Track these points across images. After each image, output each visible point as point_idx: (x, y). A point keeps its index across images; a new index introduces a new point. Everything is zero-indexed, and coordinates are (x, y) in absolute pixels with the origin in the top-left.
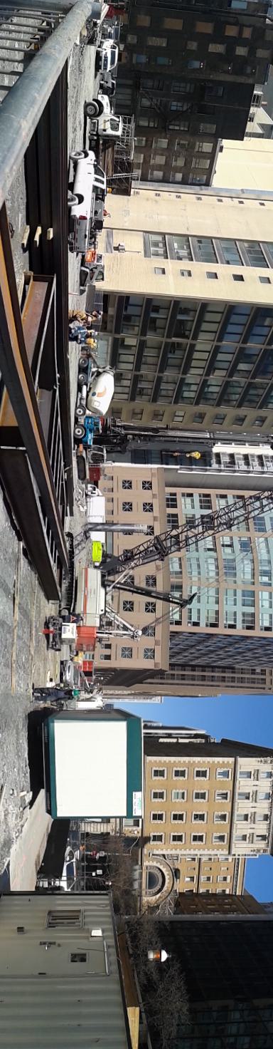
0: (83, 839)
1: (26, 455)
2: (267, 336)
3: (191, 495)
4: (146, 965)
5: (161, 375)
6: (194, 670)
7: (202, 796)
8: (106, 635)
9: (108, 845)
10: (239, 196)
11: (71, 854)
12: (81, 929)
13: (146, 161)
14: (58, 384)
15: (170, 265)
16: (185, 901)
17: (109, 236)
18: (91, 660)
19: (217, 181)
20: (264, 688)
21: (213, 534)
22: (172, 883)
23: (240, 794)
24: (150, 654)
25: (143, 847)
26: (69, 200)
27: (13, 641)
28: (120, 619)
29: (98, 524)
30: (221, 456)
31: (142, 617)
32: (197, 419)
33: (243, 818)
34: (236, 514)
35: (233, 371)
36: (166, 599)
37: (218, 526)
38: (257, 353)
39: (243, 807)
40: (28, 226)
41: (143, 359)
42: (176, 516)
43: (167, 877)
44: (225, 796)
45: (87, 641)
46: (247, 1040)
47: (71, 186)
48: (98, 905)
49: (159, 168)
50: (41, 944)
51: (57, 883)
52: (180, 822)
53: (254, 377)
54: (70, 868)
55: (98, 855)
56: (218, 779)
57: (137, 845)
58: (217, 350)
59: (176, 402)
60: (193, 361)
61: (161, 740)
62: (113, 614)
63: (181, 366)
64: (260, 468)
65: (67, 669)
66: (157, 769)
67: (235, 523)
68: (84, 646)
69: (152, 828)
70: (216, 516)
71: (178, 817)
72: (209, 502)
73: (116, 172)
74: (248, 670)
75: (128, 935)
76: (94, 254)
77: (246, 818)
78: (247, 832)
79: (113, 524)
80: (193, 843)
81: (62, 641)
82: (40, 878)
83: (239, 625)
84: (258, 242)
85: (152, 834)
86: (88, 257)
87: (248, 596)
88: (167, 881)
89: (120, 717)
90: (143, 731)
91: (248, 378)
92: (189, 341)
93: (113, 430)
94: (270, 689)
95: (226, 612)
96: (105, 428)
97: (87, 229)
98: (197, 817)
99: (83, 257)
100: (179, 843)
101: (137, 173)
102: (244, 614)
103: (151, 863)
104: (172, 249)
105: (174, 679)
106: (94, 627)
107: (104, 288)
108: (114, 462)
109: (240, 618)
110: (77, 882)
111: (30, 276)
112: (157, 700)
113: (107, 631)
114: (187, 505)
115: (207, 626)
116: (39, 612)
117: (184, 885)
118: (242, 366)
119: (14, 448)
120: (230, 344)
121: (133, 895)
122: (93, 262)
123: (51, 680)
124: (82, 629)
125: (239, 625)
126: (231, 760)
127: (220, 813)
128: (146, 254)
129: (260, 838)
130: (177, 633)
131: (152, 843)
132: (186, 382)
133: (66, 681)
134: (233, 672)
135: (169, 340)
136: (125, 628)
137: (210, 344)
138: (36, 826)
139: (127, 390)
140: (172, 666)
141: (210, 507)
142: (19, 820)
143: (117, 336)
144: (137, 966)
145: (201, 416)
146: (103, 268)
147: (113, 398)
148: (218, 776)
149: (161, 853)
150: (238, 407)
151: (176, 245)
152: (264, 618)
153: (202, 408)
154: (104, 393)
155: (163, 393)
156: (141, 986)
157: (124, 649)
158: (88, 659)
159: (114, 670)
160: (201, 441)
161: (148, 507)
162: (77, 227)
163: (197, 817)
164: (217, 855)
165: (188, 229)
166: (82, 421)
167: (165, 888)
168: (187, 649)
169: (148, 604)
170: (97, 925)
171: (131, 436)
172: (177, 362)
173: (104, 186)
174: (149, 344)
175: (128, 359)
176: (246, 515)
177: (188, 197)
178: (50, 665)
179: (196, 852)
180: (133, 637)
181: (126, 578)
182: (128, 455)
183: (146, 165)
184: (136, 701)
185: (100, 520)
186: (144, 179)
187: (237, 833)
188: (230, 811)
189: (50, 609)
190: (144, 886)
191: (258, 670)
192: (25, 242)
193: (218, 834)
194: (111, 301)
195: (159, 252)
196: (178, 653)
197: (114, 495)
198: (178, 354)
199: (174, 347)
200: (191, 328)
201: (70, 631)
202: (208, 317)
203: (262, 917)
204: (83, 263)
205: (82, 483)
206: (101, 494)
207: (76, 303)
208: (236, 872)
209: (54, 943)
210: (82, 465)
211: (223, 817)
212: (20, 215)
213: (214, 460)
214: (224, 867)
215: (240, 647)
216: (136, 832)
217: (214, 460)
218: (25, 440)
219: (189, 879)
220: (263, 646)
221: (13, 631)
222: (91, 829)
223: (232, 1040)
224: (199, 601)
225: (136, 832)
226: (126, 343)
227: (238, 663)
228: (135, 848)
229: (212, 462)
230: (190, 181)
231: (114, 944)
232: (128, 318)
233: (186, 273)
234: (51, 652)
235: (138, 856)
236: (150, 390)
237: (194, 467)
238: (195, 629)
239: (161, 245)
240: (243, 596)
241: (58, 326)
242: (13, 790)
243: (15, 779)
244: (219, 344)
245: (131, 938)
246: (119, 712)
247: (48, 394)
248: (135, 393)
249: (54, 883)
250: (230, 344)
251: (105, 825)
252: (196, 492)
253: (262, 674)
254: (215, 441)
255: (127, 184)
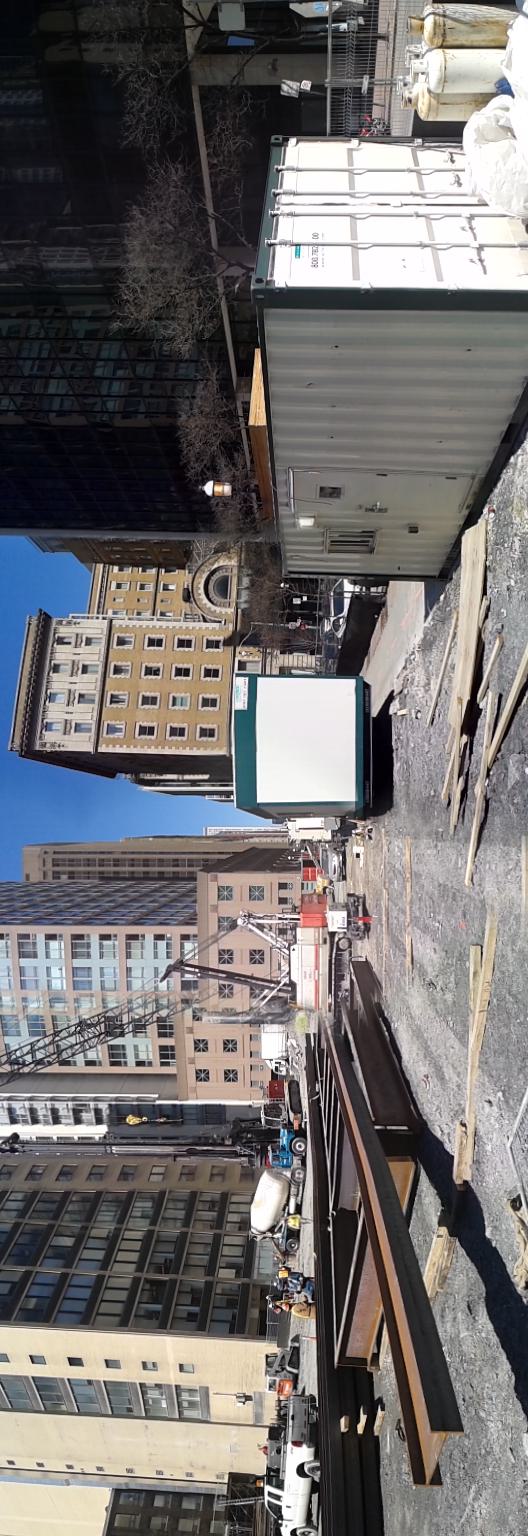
0: (319, 648)
1: (373, 1119)
2: (32, 1284)
3: (140, 1064)
4: (234, 476)
5: (185, 1230)
6: (159, 873)
7: (146, 700)
8: (286, 916)
9: (284, 637)
10: (73, 1475)
11: (336, 626)
12: (328, 528)
13: (206, 1523)
14: (330, 1218)
15: (171, 1377)
16: (178, 559)
17: (258, 1417)
18: (305, 882)
19: (104, 1496)
20: (55, 853)
21: (106, 1012)
22: (195, 583)
23: (93, 701)
24: (225, 893)
25: (235, 632)
26: (317, 1468)
27: (411, 907)
28: (269, 939)
29: (272, 1022)
30: (94, 1121)
31: (237, 943)
32: (131, 1172)
33: (90, 669)
34: (72, 1040)
35: (80, 1238)
36: (204, 971)
37: (99, 1023)
38: (46, 1260)
39: (89, 684)
40: (376, 1434)
41: (209, 1250)
42: (161, 1035)
43: (202, 591)
44: (114, 699)
45: (312, 908)
46: (98, 372)
47: (315, 1487)
48: (301, 559)
49: (187, 1514)
50: (386, 510)
51: (357, 589)
52: (180, 666)
53: (51, 1227)
54: (339, 608)
55: (298, 624)
56: (123, 722)
57: (243, 636)
58: (105, 1264)
59: (162, 1194)
60: (138, 1249)
61: (206, 777)
62: (278, 946)
63: (156, 1241)
64: (35, 1106)
65: (338, 870)
66: (210, 739)
67: (73, 1028)
68: (316, 901)
69: (220, 658)
70: (102, 1037)
71: (182, 672)
72: (112, 1056)
73: (251, 1506)
74: (80, 878)
75: (257, 516)
76: (280, 1391)
77: (85, 669)
78: (83, 649)
79: (250, 1023)
80: (162, 636)
81: (346, 906)
82: (382, 597)
83: (95, 941)
84: (47, 1412)
85: (220, 650)
86: (288, 1388)
87: (82, 982)
88: (202, 586)
89: (263, 808)
90: (234, 789)
91: (59, 1226)
92: (144, 1275)
93: (252, 1150)
94: (46, 853)
95: (115, 957)
96: (263, 1153)
97: (290, 1429)
98: (156, 672)
99: (295, 1388)
100: (183, 637)
101: (219, 1506)
102: (89, 956)
103: (224, 610)
104: (169, 1399)
105: (189, 860)
106: (304, 927)
107: (265, 1344)
108: (250, 1106)
109: (95, 950)
110: (330, 590)
111: (372, 1365)
112: (212, 831)
113: (285, 922)
114: (145, 1049)
115: (143, 936)
116: (378, 945)
117: (179, 579)
118: (69, 1242)
119: (389, 1128)
120: (86, 1272)
121: (251, 568)
122: (281, 1380)
123: (358, 855)
124: (320, 924)
125: (95, 941)
126: (102, 749)
127: (122, 676)
128: (205, 1391)
129: (66, 640)
130: (187, 924)
131: (221, 638)
132: (148, 1221)
133: (338, 854)
134: (102, 873)
135: (173, 1276)
136: (261, 927)
137: (115, 1272)
138: (385, 666)
139: (233, 1208)
140: (192, 878)
141: (111, 1047)
142: (409, 677)
143: (246, 1280)
144: (247, 476)
145: (125, 1175)
146: (267, 1372)
147: (253, 1195)
148: (123, 727)
149: (207, 625)
150: (70, 1193)
151: (164, 1405)
152: (57, 952)
153: (123, 1188)
154: (266, 1201)
155: (181, 1205)
156: (244, 451)
157: (261, 898)
158: (310, 883)
159: (273, 870)
160: (125, 1141)
161: (201, 1046)
162: (305, 1431)
163: (156, 672)
164: (130, 619)
165: (146, 1427)
166: (296, 1162)
167: (205, 576)
168: (172, 901)
169: (230, 961)
170: (306, 533)
171: (227, 1142)
172: (161, 1247)
173: (268, 1489)
174: (202, 1271)
175: (231, 1250)
176: (57, 1038)
177: (146, 1472)
178: (360, 874)
179: (160, 623)
180: (250, 916)
181: (262, 996)
182: (230, 1117)
183: (206, 1517)
184: (242, 829)
185: (268, 1028)
186: (209, 1498)
187: (99, 648)
188: (108, 680)
189: (364, 950)
190: (235, 580)
191: (64, 878)
192: (380, 1413)
193: (126, 647)
194: (255, 1327)
195: (187, 1394)
196: (184, 895)
197: (248, 1061)
198: (160, 1259)
199: (166, 1267)
200: (141, 1294)
201: (337, 920)
202: (118, 1308)
203: (67, 534)
204: (295, 1379)
205: (293, 1076)
206: (268, 1062)
207: (304, 1325)
208: (102, 600)
209: (367, 510)
210: (295, 1101)
211: (117, 670)
212: (388, 1450)
213: (105, 1113)
214: (120, 603)
215: (92, 908)
216: (243, 653)
217: (105, 1113)
218: (375, 1139)
219: (171, 587)
220: (59, 912)
221: (411, 920)
222: (309, 660)
223: (120, 373)
224: (156, 969)
225: (243, 653)
226: (234, 1271)
227: (95, 887)
228: (245, 632)
229: (108, 1111)
230: (143, 1495)
231: (280, 508)
232: (231, 1304)
233: (150, 1366)
234: (360, 892)
235: (242, 621)
236: (200, 1208)
237: (135, 1103)
238: (160, 930)
239: (185, 1404)
240: (90, 982)
241: (329, 1295)
242: (417, 718)
243: (413, 732)
244: (102, 1272)
245: (252, 513)
246: (266, 815)
247: (345, 1203)
248: (222, 1204)
249: (361, 589)
250: (86, 1272)
251: (286, 665)
252: (131, 1068)
253: (58, 873)
254: (104, 1142)
255: (234, 1489)
